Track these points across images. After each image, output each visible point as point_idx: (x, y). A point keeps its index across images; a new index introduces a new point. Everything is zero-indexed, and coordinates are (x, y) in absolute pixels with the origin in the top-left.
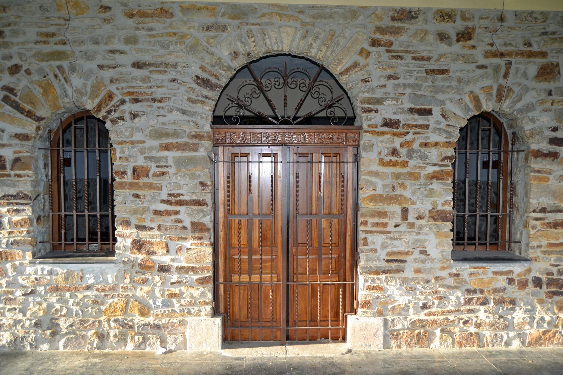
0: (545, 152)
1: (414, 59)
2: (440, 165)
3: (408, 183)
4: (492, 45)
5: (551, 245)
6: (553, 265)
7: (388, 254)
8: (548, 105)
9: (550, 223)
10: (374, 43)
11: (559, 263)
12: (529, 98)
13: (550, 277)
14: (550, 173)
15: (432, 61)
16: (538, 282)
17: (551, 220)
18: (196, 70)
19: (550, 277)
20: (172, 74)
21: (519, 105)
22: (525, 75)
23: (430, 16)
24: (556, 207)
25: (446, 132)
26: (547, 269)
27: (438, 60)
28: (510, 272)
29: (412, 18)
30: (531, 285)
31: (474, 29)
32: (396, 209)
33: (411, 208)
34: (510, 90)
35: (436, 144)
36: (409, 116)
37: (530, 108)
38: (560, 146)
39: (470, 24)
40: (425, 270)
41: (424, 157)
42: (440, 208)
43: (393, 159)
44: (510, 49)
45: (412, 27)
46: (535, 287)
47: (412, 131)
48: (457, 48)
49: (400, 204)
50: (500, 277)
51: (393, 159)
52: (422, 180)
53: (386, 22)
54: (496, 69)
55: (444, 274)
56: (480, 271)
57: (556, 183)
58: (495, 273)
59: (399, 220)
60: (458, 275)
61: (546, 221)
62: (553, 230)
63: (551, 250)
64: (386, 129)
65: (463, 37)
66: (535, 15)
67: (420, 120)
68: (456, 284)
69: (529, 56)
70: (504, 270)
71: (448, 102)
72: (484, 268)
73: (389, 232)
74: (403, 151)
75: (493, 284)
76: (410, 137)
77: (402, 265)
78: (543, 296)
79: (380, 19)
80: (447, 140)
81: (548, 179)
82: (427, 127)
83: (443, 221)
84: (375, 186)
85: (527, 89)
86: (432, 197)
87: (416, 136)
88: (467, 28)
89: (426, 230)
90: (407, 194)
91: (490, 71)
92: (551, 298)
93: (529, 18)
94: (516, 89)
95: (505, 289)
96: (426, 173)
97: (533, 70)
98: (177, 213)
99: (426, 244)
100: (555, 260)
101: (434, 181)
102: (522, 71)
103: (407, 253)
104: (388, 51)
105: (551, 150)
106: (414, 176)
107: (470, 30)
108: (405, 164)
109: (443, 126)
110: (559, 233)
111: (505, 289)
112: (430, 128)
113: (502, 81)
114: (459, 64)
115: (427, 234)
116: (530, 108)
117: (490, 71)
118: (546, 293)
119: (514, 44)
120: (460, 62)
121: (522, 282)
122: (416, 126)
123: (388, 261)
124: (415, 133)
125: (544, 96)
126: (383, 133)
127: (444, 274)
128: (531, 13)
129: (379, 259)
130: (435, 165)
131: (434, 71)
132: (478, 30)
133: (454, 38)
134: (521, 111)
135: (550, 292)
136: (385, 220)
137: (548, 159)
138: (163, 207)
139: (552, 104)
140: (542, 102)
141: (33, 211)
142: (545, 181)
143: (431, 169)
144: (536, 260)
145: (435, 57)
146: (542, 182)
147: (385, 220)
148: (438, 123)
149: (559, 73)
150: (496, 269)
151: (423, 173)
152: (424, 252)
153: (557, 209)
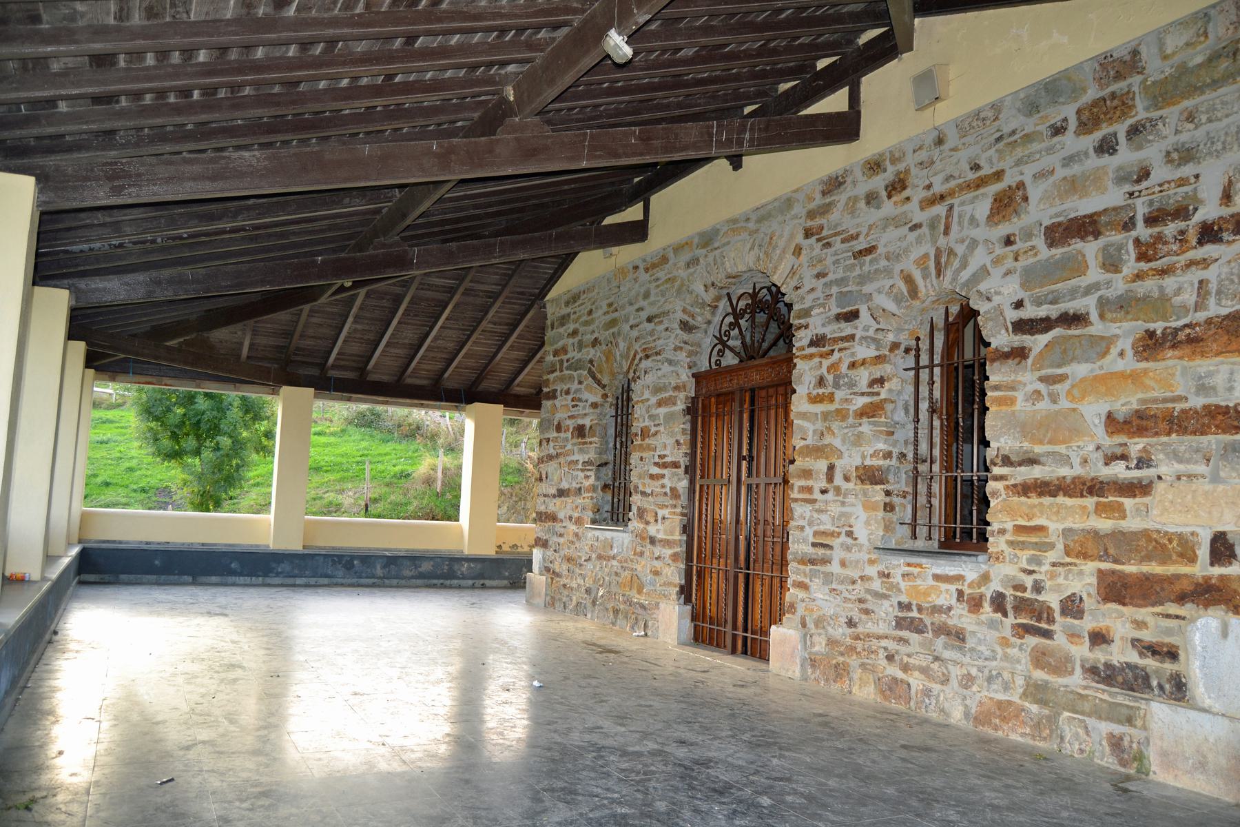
0: (1006, 349)
1: (843, 241)
2: (868, 394)
3: (835, 426)
4: (929, 187)
5: (1019, 529)
6: (1024, 571)
7: (816, 534)
8: (1009, 263)
9: (1015, 486)
10: (808, 234)
11: (1036, 568)
12: (980, 258)
13: (1019, 594)
14: (1013, 389)
15: (861, 238)
16: (999, 603)
17: (1019, 480)
18: (680, 315)
19: (1019, 594)
20: (571, 327)
21: (965, 275)
22: (973, 221)
23: (858, 173)
24: (1026, 452)
25: (874, 340)
26: (1014, 577)
27: (867, 235)
28: (960, 578)
29: (841, 184)
30: (987, 607)
31: (907, 171)
32: (822, 465)
33: (839, 464)
34: (951, 252)
35: (864, 362)
36: (835, 326)
37: (984, 272)
38: (1032, 334)
39: (901, 167)
40: (851, 562)
41: (851, 385)
42: (868, 462)
43: (821, 391)
44: (953, 184)
45: (841, 197)
46: (996, 611)
47: (836, 347)
48: (889, 208)
49: (827, 458)
50: (944, 586)
51: (821, 391)
52: (851, 420)
53: (819, 200)
54: (933, 226)
55: (872, 571)
56: (916, 570)
57: (1028, 407)
58: (937, 577)
59: (823, 484)
60: (888, 576)
61: (1012, 482)
62: (1023, 499)
63: (1021, 539)
64: (813, 350)
65: (894, 189)
66: (982, 115)
67: (847, 329)
68: (884, 591)
69: (978, 187)
70: (951, 573)
71: (875, 295)
72: (920, 566)
73: (815, 501)
74: (830, 378)
75: (934, 596)
76: (836, 355)
77: (828, 552)
78: (1007, 632)
79: (811, 199)
80: (877, 353)
81: (1012, 401)
82: (851, 337)
83: (872, 484)
84: (805, 433)
85: (974, 243)
86: (861, 445)
87: (842, 354)
88: (899, 173)
89: (851, 499)
90: (837, 442)
91: (925, 229)
92: (1022, 637)
93: (975, 124)
94: (960, 250)
95: (950, 609)
96: (855, 408)
97: (983, 208)
98: (663, 476)
99: (852, 521)
100: (1029, 561)
101: (865, 420)
102: (968, 216)
103: (832, 534)
104: (818, 240)
105: (1016, 345)
106: (841, 414)
107: (902, 176)
108: (831, 397)
109: (871, 333)
110: (1035, 506)
111: (950, 609)
112: (857, 338)
113: (942, 241)
114: (892, 234)
115: (853, 505)
116: (984, 272)
117: (925, 229)
118: (1013, 626)
119: (956, 174)
120: (892, 228)
121: (974, 599)
122: (842, 339)
123: (814, 545)
124: (840, 350)
125: (1000, 250)
126: (811, 356)
127: (872, 571)
128: (977, 114)
129: (805, 541)
130: (863, 394)
131: (860, 251)
132: (914, 171)
133: (884, 194)
134: (967, 284)
135: (1020, 625)
136: (810, 483)
137: (1010, 361)
138: (655, 470)
139: (1016, 259)
140: (997, 261)
141: (597, 478)
142: (1007, 405)
143: (861, 402)
144: (998, 558)
145: (864, 230)
146: (1004, 408)
147: (810, 483)
148: (866, 329)
149: (1026, 199)
150: (938, 571)
151: (853, 408)
152: (849, 534)
153: (1026, 456)
